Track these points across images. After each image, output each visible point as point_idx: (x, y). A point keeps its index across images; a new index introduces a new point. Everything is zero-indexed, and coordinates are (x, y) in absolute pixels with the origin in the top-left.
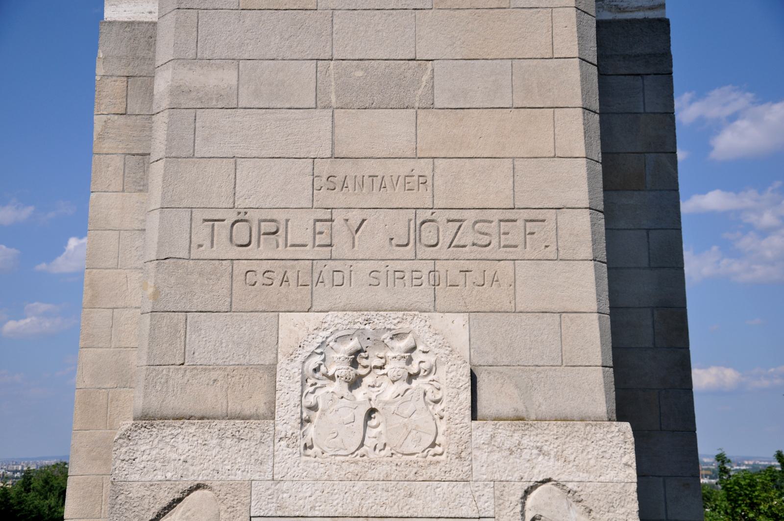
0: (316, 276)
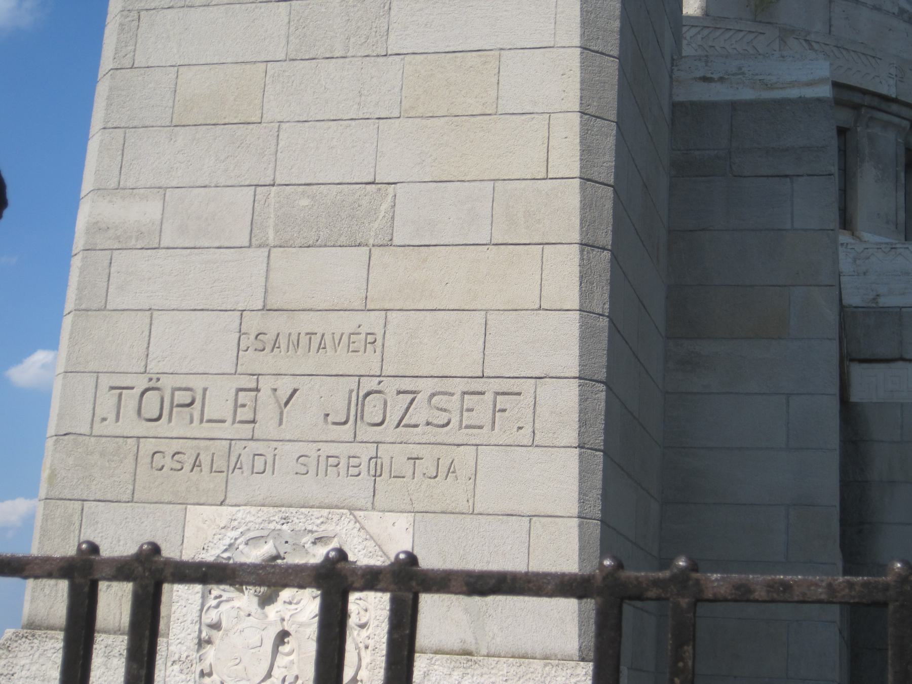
0: (233, 460)
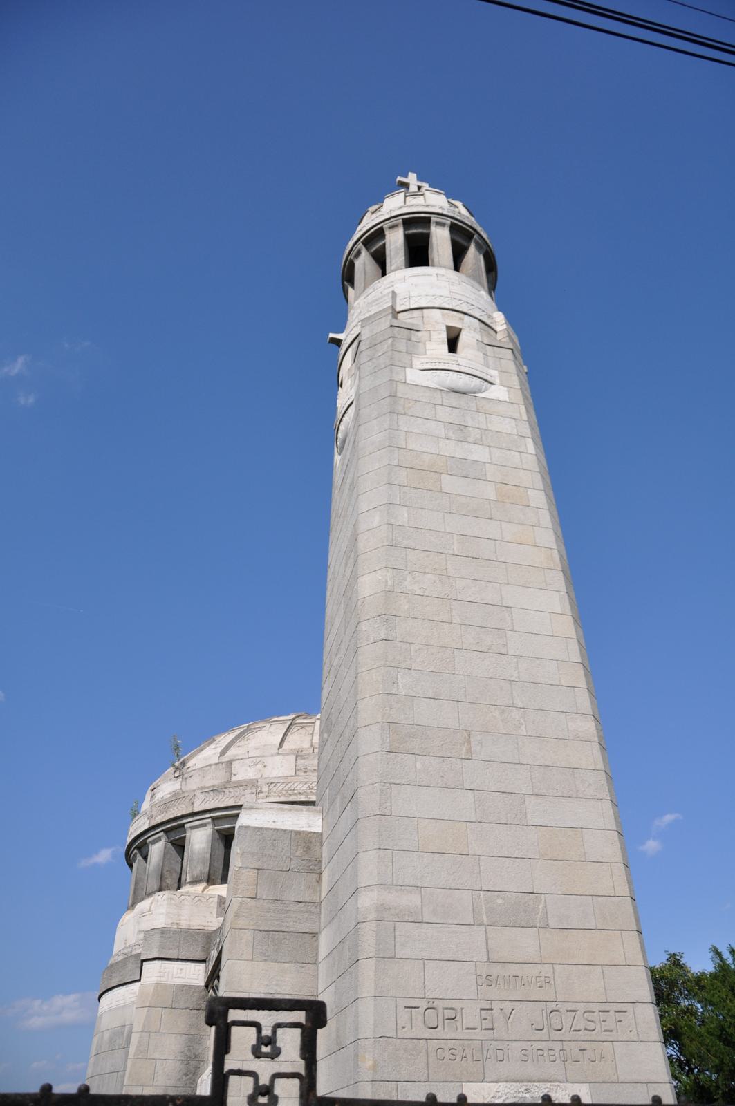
0: (485, 1053)
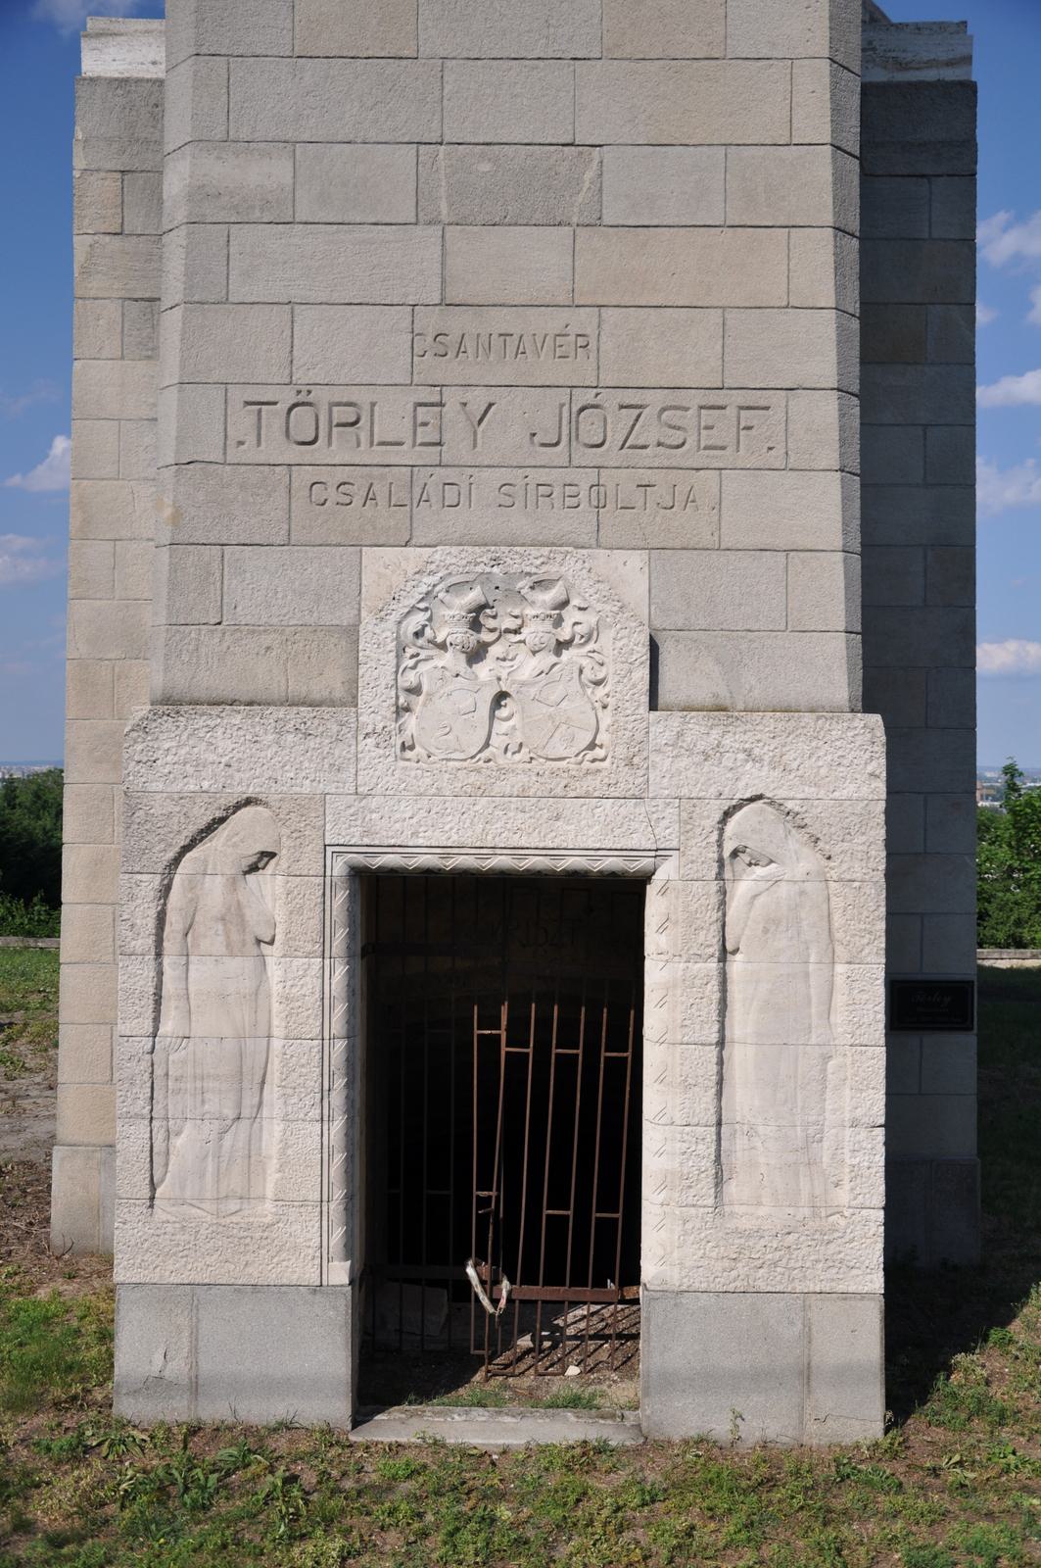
0: (417, 491)
